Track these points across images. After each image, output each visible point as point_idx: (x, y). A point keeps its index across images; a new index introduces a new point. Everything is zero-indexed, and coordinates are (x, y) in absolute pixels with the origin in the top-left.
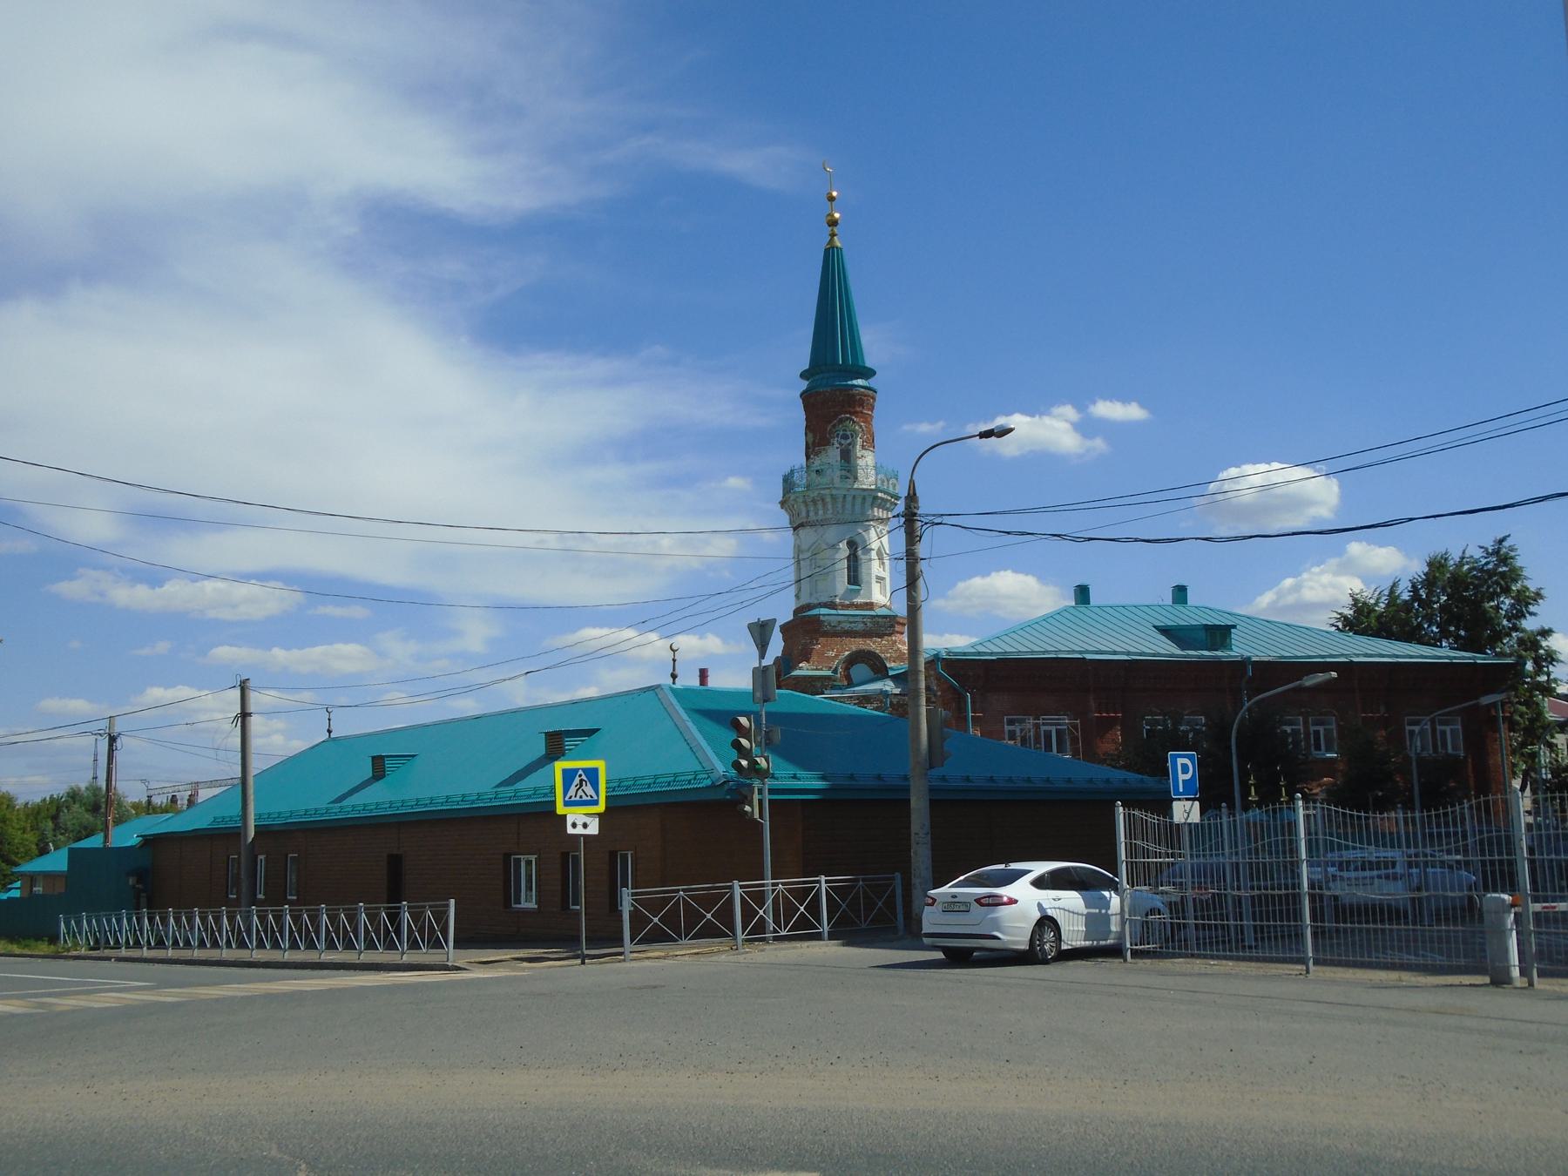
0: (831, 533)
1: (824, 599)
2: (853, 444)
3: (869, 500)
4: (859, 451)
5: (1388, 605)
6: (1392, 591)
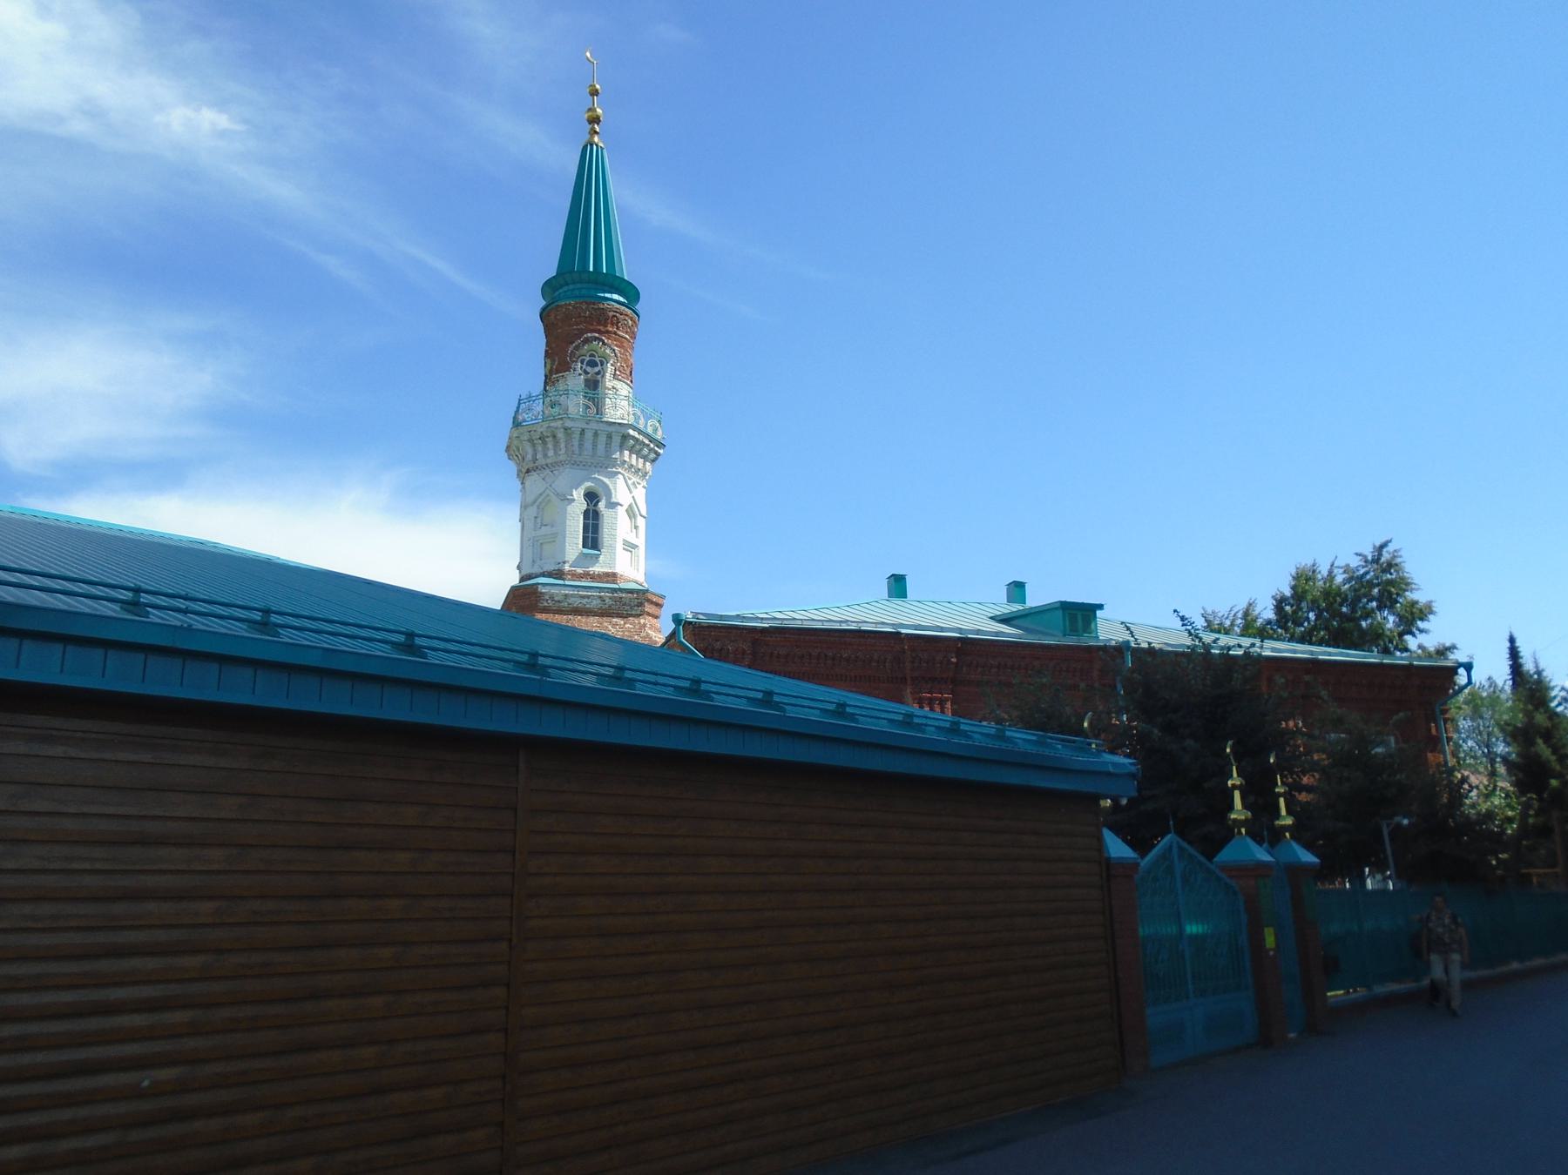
0: (562, 478)
1: (550, 567)
2: (602, 373)
3: (617, 440)
4: (609, 381)
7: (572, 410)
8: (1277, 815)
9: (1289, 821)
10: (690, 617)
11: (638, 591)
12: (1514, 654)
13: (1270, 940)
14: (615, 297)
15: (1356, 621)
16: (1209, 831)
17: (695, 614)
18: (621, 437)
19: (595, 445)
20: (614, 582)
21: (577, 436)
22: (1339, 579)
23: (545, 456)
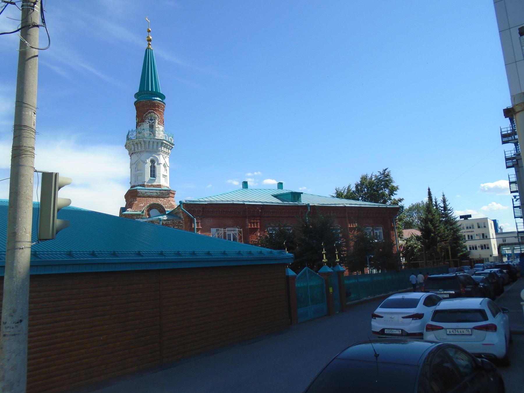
0: (143, 156)
1: (140, 183)
2: (154, 123)
3: (160, 144)
4: (157, 125)
5: (347, 193)
6: (348, 189)
7: (146, 135)
8: (336, 259)
9: (338, 260)
10: (184, 202)
11: (167, 190)
12: (430, 194)
13: (331, 290)
14: (158, 99)
15: (377, 191)
16: (316, 264)
17: (186, 201)
18: (161, 143)
19: (153, 146)
20: (160, 187)
21: (147, 143)
22: (373, 179)
23: (138, 149)
